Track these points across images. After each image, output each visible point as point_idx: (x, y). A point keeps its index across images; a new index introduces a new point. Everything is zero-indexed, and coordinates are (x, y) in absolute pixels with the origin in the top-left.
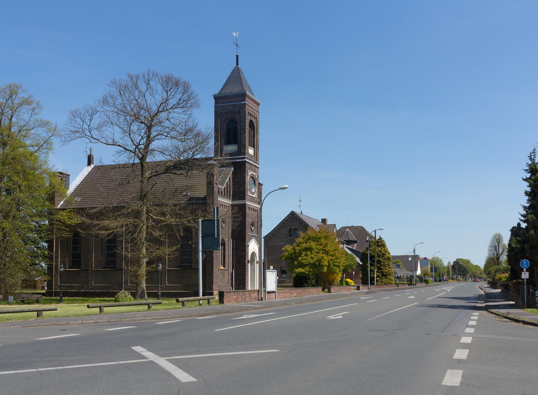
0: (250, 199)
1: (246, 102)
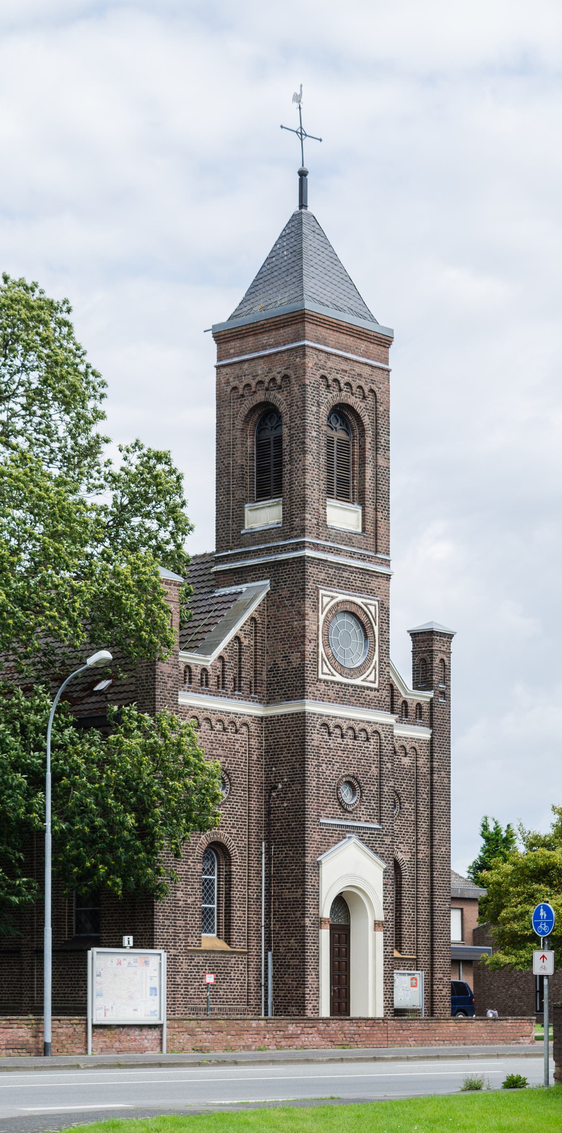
0: (330, 692)
1: (306, 343)
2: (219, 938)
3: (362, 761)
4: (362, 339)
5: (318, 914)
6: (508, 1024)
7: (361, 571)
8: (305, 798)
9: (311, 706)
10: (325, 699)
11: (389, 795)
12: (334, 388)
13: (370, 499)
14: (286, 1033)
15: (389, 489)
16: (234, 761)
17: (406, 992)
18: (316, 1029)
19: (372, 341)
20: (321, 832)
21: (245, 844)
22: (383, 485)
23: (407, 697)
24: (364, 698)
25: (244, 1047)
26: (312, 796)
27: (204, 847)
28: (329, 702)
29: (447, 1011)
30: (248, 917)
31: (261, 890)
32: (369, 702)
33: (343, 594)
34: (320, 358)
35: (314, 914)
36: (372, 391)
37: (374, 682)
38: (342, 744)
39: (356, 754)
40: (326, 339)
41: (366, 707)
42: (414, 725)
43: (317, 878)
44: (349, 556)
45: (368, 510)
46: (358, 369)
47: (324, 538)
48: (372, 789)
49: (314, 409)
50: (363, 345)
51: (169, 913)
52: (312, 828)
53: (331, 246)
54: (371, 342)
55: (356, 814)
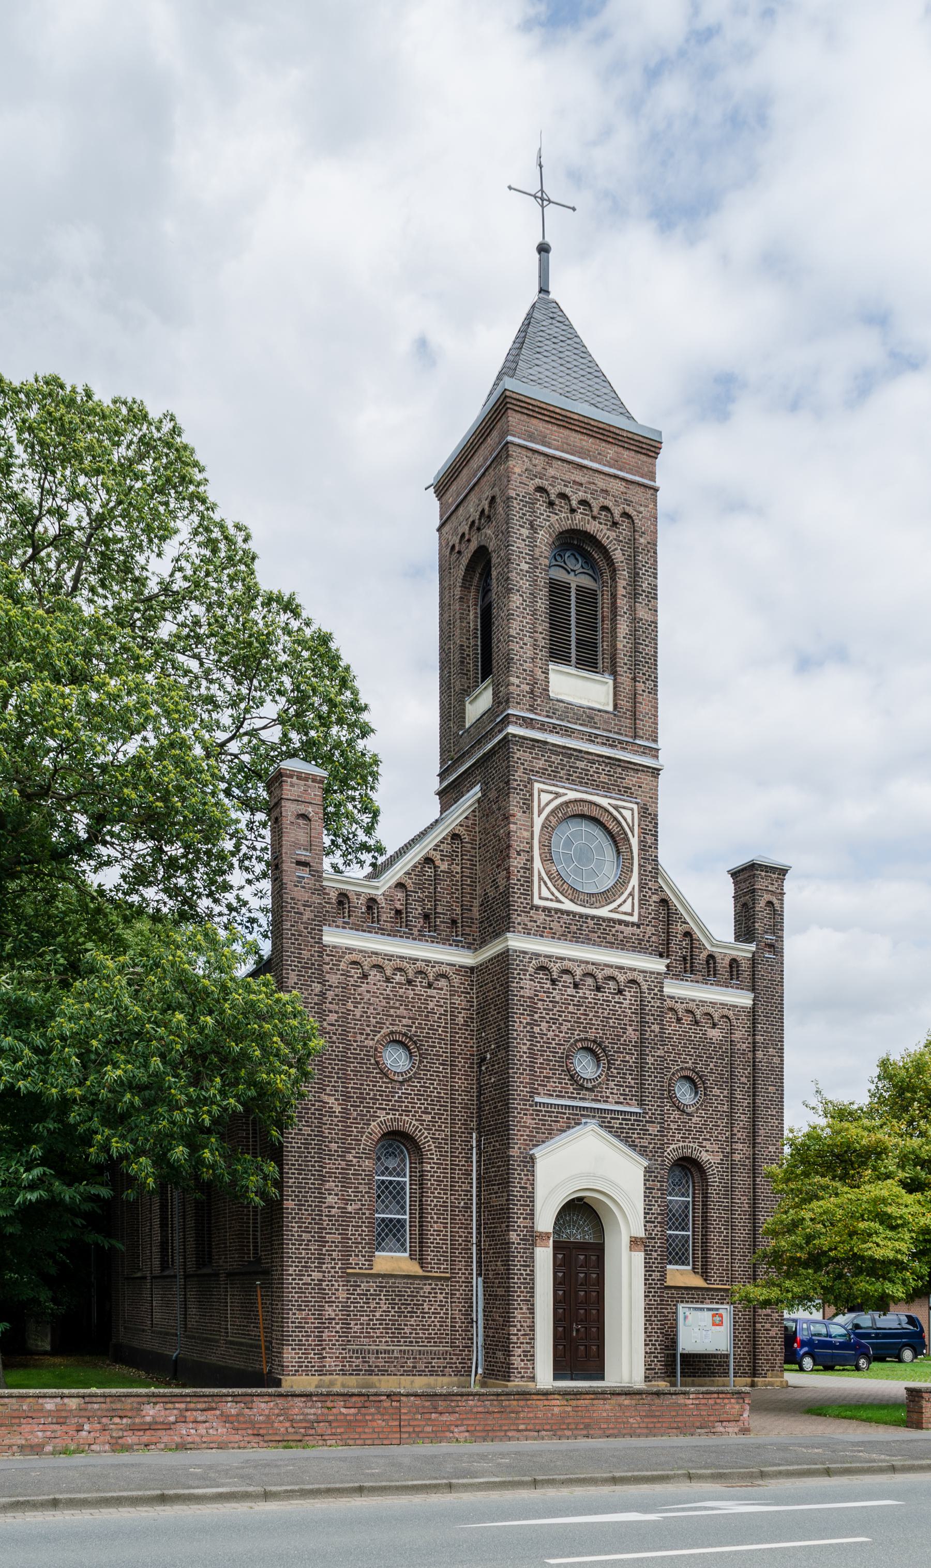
2: (411, 1259)
3: (611, 1021)
4: (609, 442)
5: (533, 1227)
6: (690, 1402)
7: (607, 761)
8: (508, 1068)
9: (516, 942)
10: (545, 934)
11: (655, 1069)
12: (562, 507)
13: (626, 664)
14: (137, 1420)
15: (656, 652)
16: (426, 1024)
17: (704, 1332)
18: (218, 1412)
19: (626, 445)
20: (537, 1115)
21: (446, 1135)
22: (646, 645)
23: (714, 949)
24: (613, 935)
25: (21, 1447)
26: (521, 1065)
27: (376, 1137)
28: (553, 938)
29: (777, 1356)
30: (451, 1232)
31: (471, 1196)
32: (622, 941)
33: (576, 790)
34: (534, 462)
35: (524, 1227)
36: (625, 515)
37: (631, 915)
38: (575, 997)
39: (600, 1011)
40: (545, 437)
41: (617, 948)
42: (727, 987)
43: (531, 1178)
44: (587, 740)
45: (620, 679)
46: (601, 483)
47: (545, 713)
48: (627, 1059)
49: (525, 532)
50: (611, 452)
51: (310, 1223)
52: (521, 1109)
53: (584, 346)
54: (623, 447)
55: (601, 1092)
